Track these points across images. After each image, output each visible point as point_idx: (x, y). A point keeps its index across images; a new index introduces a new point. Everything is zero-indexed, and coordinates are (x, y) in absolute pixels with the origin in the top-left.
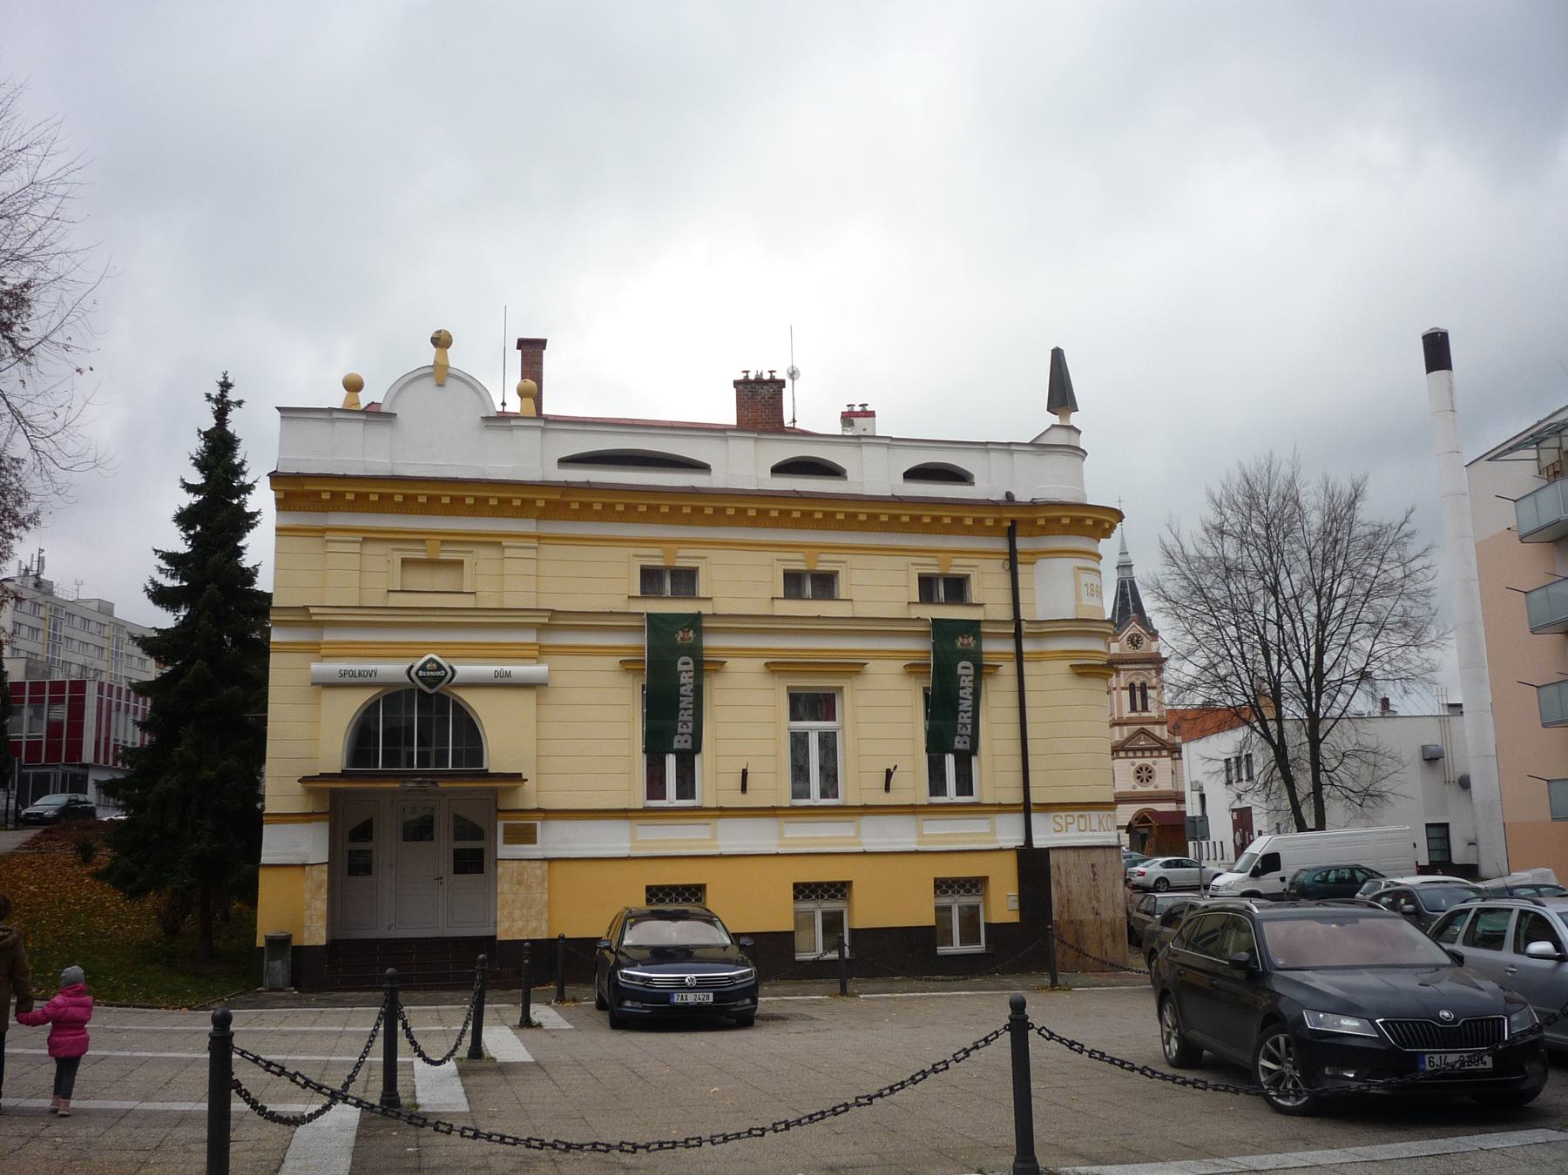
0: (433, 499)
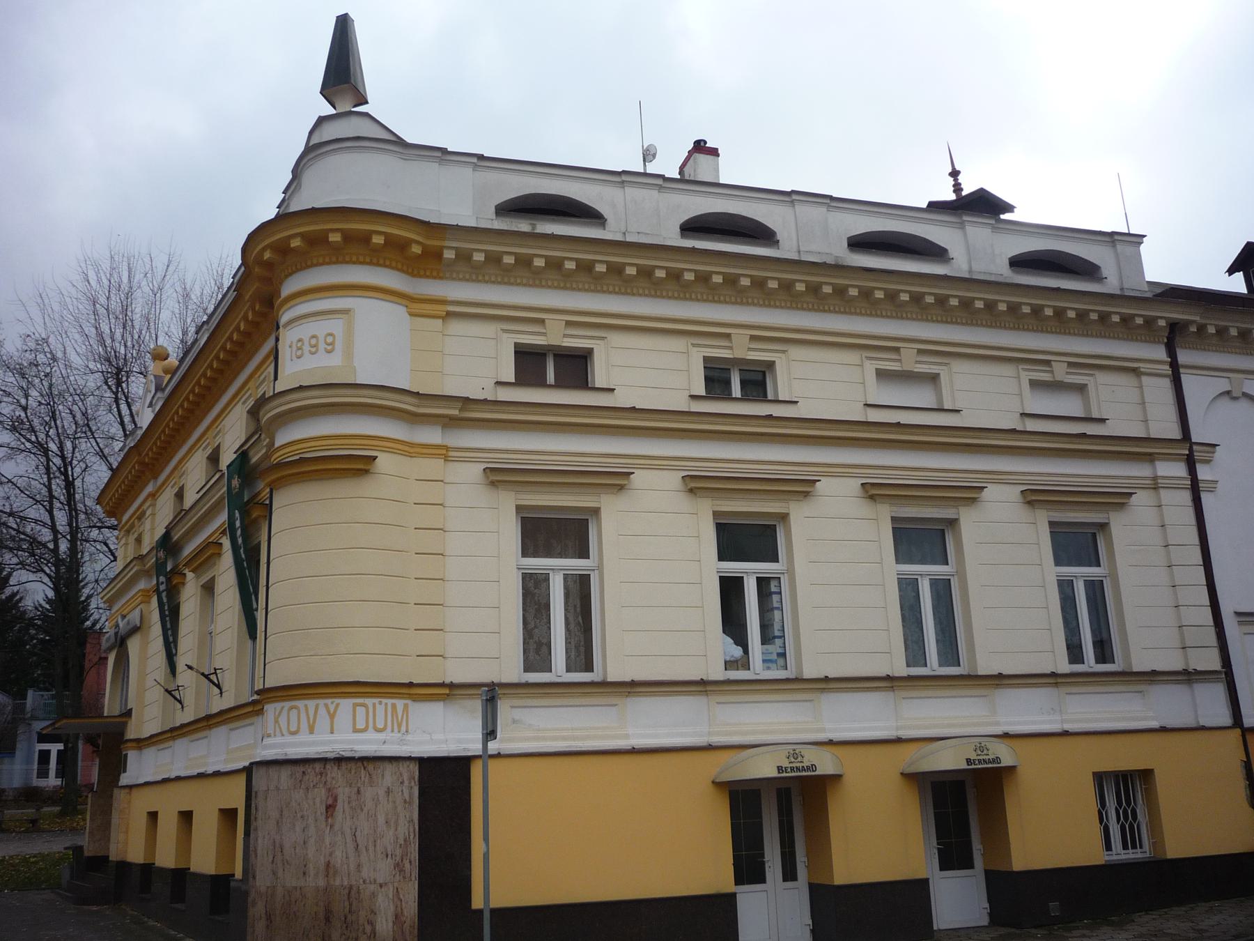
0: (646, 273)
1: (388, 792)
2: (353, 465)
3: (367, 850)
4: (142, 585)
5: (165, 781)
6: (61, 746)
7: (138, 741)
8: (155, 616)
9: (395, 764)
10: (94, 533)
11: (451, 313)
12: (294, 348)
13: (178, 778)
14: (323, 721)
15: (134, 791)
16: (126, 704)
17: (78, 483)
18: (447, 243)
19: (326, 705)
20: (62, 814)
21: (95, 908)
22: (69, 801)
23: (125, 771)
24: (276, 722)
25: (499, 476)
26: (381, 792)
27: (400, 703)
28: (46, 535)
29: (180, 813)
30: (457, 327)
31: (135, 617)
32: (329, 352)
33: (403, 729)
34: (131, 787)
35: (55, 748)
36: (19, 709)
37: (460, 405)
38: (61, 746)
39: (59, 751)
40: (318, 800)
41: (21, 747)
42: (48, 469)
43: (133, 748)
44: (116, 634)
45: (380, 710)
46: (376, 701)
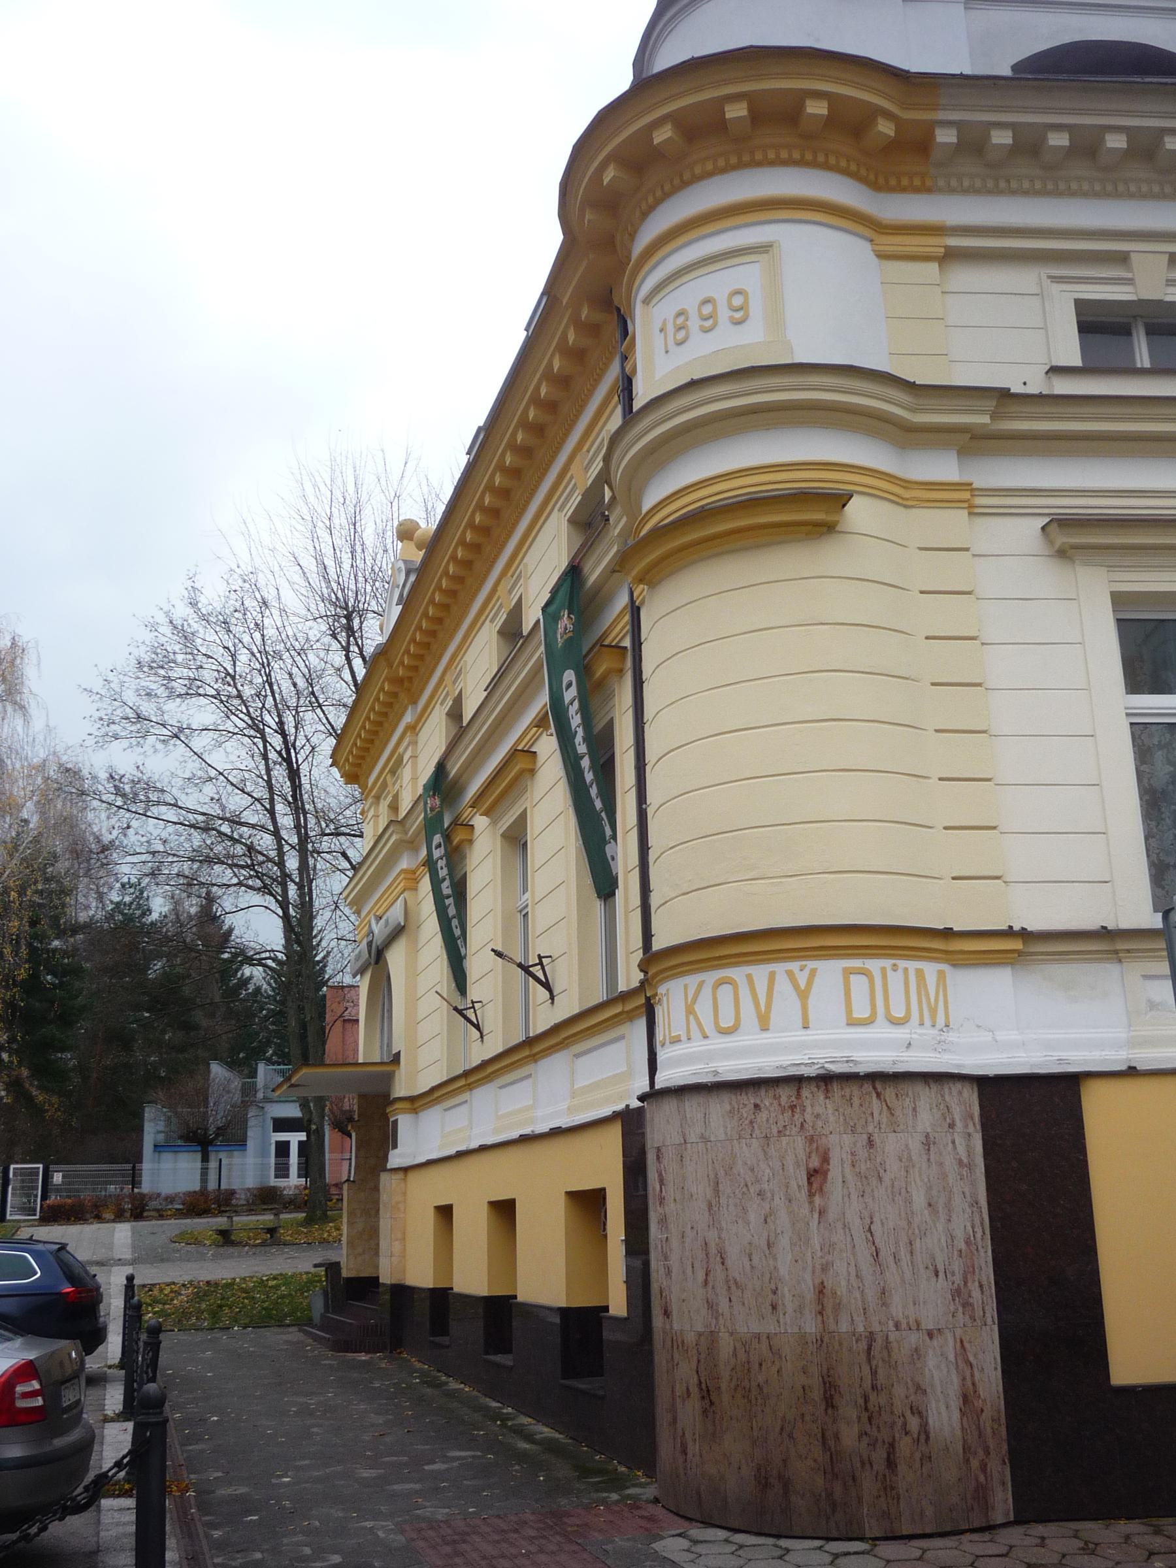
1: (928, 1143)
2: (805, 513)
3: (897, 1260)
4: (405, 863)
5: (460, 1155)
6: (302, 1136)
7: (412, 1099)
8: (428, 907)
9: (935, 1087)
10: (326, 843)
11: (955, 252)
12: (670, 328)
13: (483, 1149)
14: (786, 1003)
15: (412, 1177)
16: (389, 1045)
17: (304, 769)
18: (941, 115)
19: (790, 974)
20: (309, 1221)
21: (363, 1357)
22: (317, 1205)
23: (395, 1146)
24: (690, 1011)
25: (1076, 535)
26: (915, 1145)
27: (931, 969)
28: (266, 842)
29: (492, 1204)
30: (965, 277)
31: (396, 914)
32: (738, 323)
33: (941, 1021)
34: (406, 1170)
35: (295, 1138)
36: (249, 1090)
37: (991, 404)
38: (302, 1136)
39: (300, 1143)
40: (790, 1161)
41: (253, 1136)
42: (265, 757)
43: (404, 1111)
44: (370, 944)
45: (895, 981)
46: (887, 963)
